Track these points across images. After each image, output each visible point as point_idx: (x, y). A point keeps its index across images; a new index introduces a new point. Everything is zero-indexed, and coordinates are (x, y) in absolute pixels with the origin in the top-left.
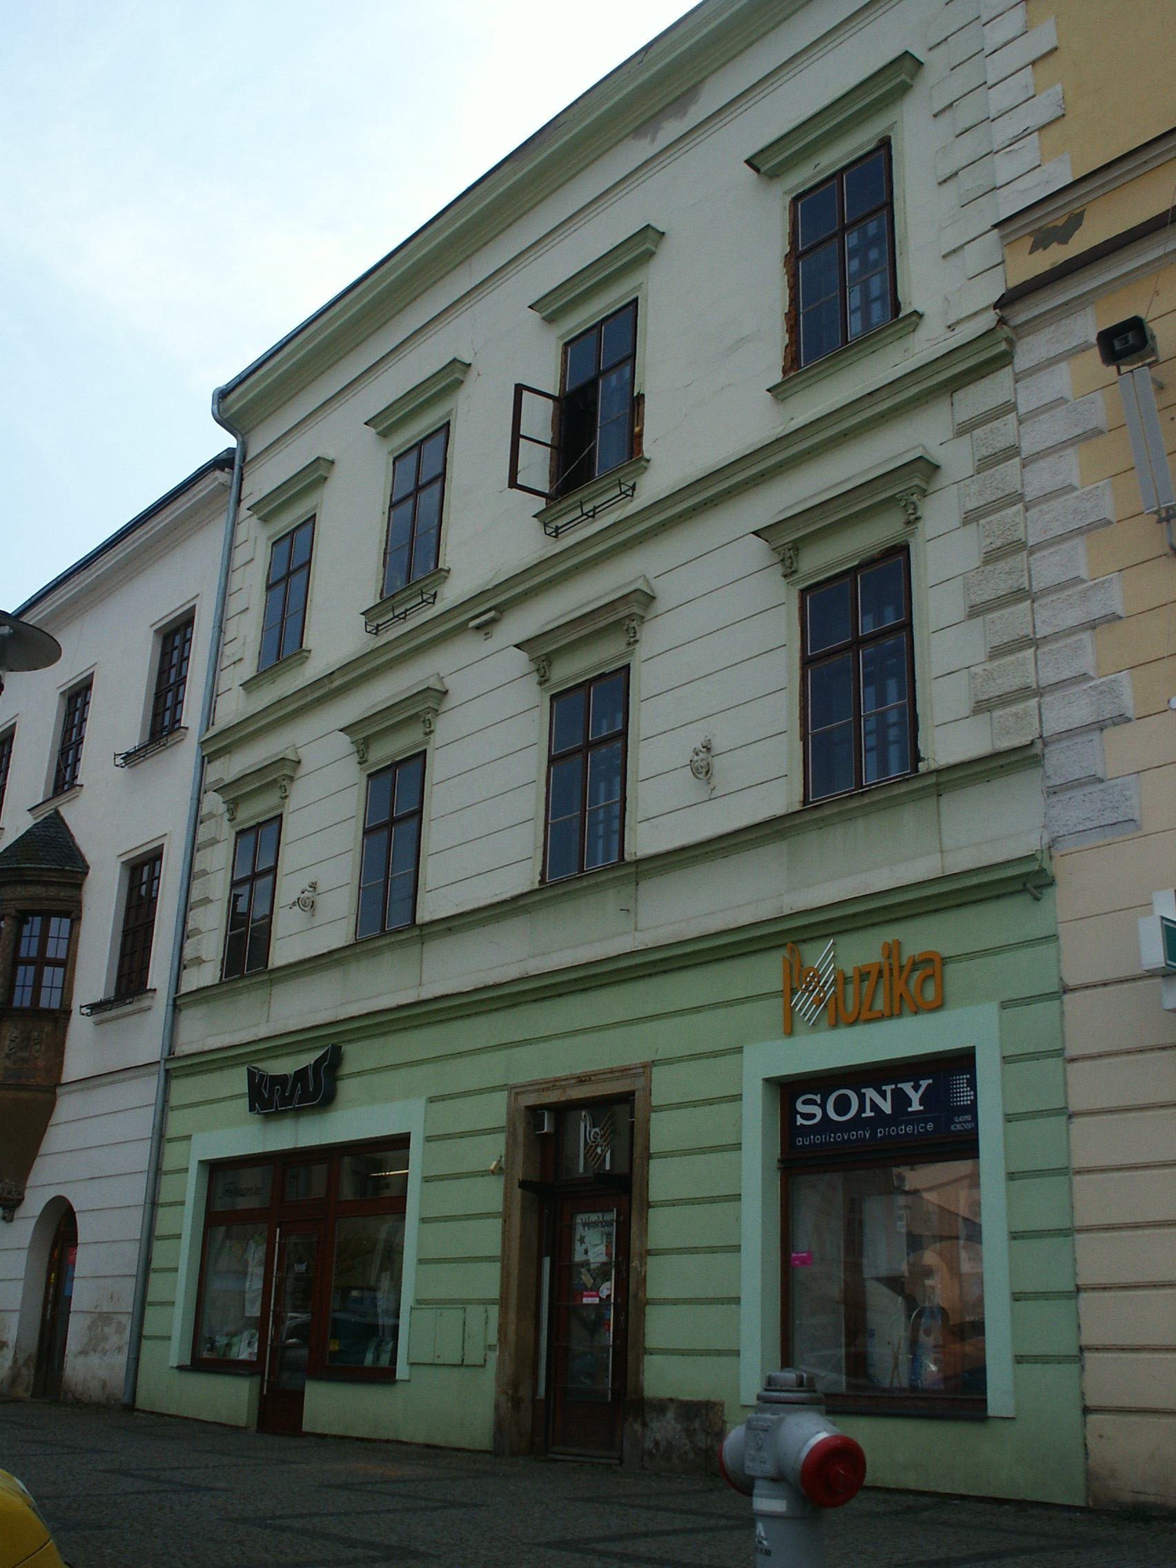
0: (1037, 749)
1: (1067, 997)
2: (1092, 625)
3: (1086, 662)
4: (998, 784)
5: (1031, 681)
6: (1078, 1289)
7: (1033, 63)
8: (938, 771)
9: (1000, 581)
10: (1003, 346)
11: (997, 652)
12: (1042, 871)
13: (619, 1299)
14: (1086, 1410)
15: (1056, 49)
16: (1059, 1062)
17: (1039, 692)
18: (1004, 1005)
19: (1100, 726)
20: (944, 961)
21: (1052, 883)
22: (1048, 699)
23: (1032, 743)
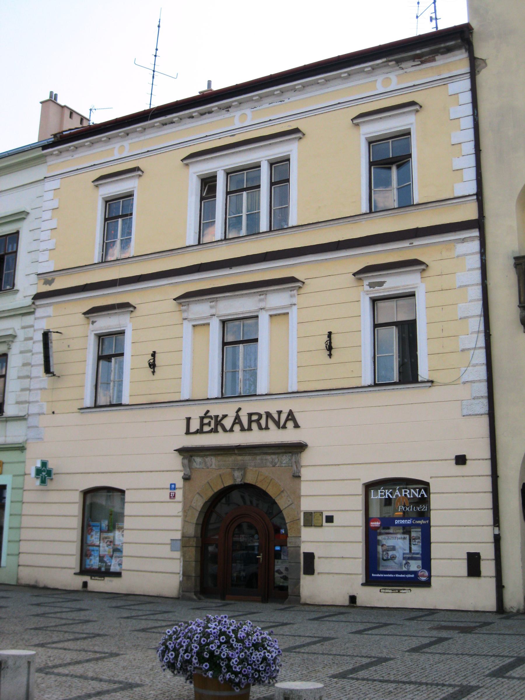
0: (26, 417)
1: (26, 476)
2: (41, 389)
3: (38, 398)
4: (368, 179)
5: (27, 399)
6: (20, 540)
7: (51, 229)
8: (6, 418)
9: (24, 373)
10: (33, 310)
11: (23, 390)
12: (23, 447)
13: (283, 532)
14: (19, 566)
15: (56, 228)
16: (21, 491)
17: (29, 402)
18: (14, 476)
19: (39, 414)
20: (3, 463)
21: (25, 449)
22: (31, 405)
23: (25, 416)
